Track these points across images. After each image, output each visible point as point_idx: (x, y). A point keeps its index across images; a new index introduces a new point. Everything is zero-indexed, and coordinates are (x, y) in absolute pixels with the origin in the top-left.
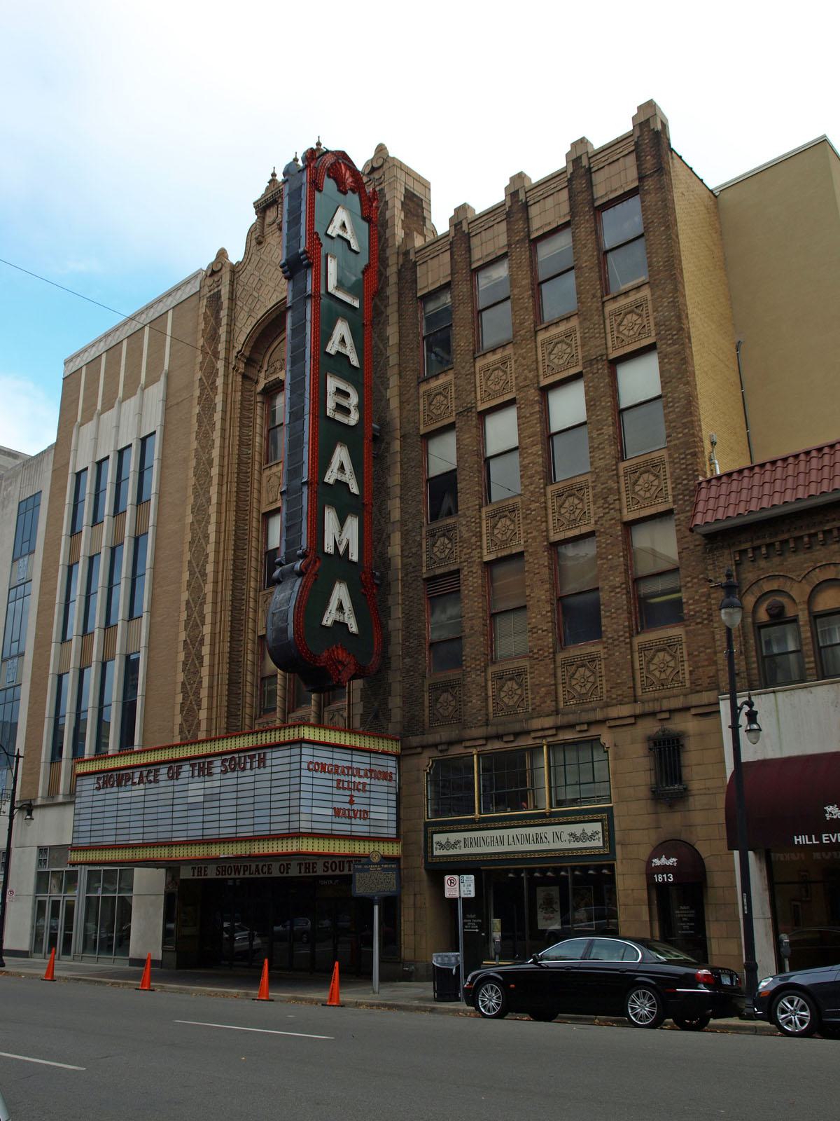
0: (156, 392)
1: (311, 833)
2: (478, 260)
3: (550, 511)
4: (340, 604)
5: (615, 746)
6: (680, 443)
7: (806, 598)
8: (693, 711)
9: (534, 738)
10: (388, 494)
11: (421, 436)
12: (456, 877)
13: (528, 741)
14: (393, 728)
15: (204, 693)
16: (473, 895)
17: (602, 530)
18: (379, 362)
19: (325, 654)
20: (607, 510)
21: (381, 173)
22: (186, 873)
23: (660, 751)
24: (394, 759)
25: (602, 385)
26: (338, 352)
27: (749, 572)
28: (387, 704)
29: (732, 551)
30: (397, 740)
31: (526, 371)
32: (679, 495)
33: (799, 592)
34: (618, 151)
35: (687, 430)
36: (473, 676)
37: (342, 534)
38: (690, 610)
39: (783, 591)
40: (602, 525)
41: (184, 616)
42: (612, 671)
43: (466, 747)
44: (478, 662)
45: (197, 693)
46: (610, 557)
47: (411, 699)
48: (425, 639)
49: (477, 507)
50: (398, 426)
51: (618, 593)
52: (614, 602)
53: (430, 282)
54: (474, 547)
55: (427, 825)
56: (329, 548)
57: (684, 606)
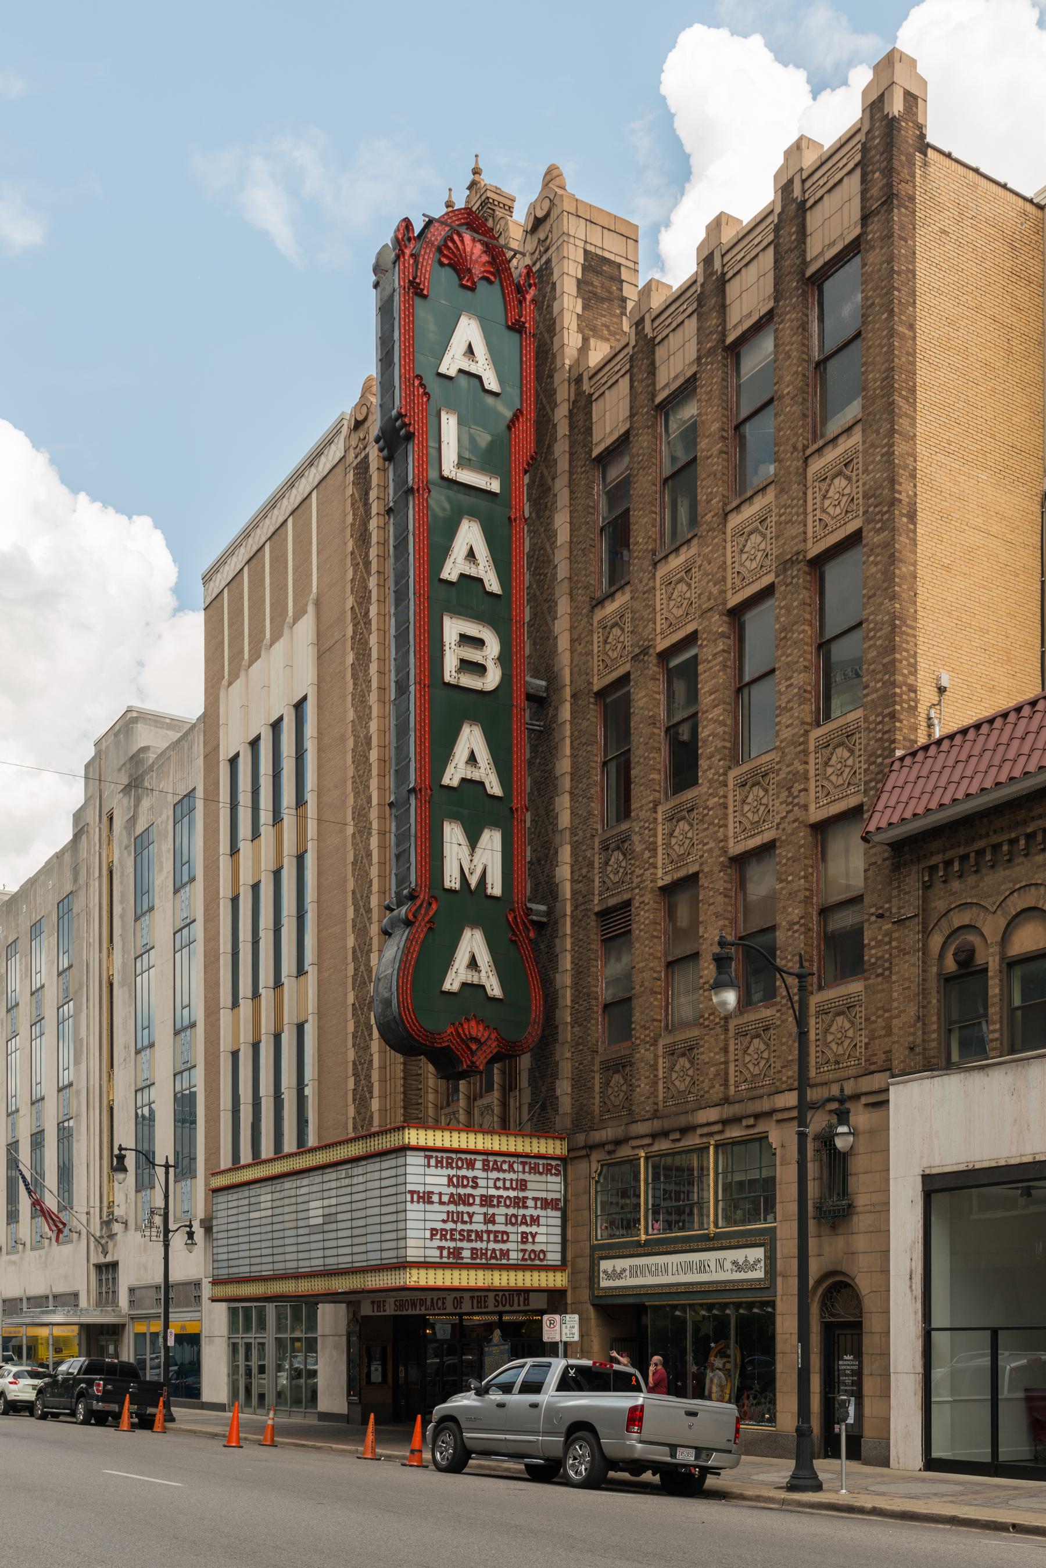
0: (305, 629)
1: (425, 1262)
2: (663, 388)
3: (731, 809)
4: (472, 960)
5: (782, 1146)
6: (879, 698)
7: (998, 938)
8: (864, 1100)
9: (701, 1136)
10: (556, 787)
11: (595, 694)
12: (557, 1317)
13: (693, 1140)
15: (375, 1076)
17: (784, 838)
18: (546, 575)
19: (450, 1030)
20: (790, 807)
21: (547, 230)
22: (366, 1310)
23: (830, 1154)
25: (796, 604)
26: (462, 575)
27: (940, 899)
28: (554, 1090)
29: (921, 866)
30: (562, 1139)
31: (711, 584)
32: (871, 781)
33: (992, 926)
34: (840, 165)
35: (887, 677)
36: (643, 1051)
37: (473, 858)
38: (871, 956)
39: (975, 927)
40: (784, 829)
41: (351, 971)
42: (784, 1044)
43: (633, 1148)
44: (647, 1032)
45: (368, 1077)
46: (790, 878)
47: (580, 1083)
48: (597, 999)
49: (651, 805)
50: (568, 682)
51: (796, 931)
52: (791, 945)
53: (608, 430)
54: (647, 866)
55: (593, 1248)
56: (451, 880)
57: (866, 949)
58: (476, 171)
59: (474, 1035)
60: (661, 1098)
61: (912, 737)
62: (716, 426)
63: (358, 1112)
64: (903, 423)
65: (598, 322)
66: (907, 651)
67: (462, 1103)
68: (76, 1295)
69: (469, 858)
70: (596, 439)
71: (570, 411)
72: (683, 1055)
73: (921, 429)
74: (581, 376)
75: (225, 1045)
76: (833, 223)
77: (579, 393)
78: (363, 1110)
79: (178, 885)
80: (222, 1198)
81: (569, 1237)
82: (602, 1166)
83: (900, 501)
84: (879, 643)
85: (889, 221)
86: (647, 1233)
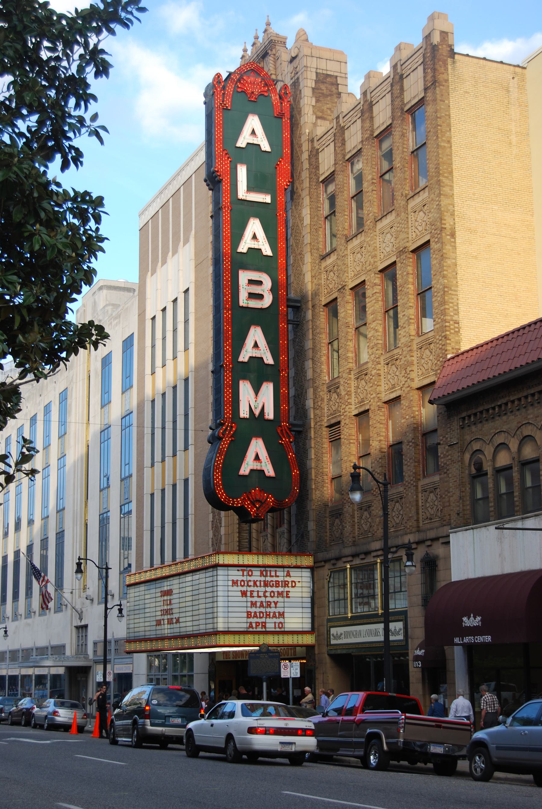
4: (257, 457)
7: (491, 458)
8: (441, 540)
9: (374, 557)
14: (311, 546)
16: (299, 676)
24: (309, 570)
33: (488, 451)
34: (409, 67)
37: (256, 400)
38: (442, 462)
49: (348, 371)
56: (244, 413)
58: (268, 24)
59: (258, 498)
60: (356, 534)
61: (457, 347)
62: (370, 177)
63: (214, 535)
64: (446, 190)
65: (325, 108)
66: (452, 303)
67: (269, 530)
68: (63, 647)
69: (254, 400)
70: (321, 172)
71: (309, 156)
72: (366, 510)
73: (456, 190)
74: (313, 139)
75: (147, 490)
76: (414, 88)
77: (313, 148)
78: (217, 534)
79: (124, 390)
80: (132, 591)
81: (316, 614)
82: (331, 572)
83: (445, 228)
84: (439, 299)
85: (434, 93)
86: (352, 613)
